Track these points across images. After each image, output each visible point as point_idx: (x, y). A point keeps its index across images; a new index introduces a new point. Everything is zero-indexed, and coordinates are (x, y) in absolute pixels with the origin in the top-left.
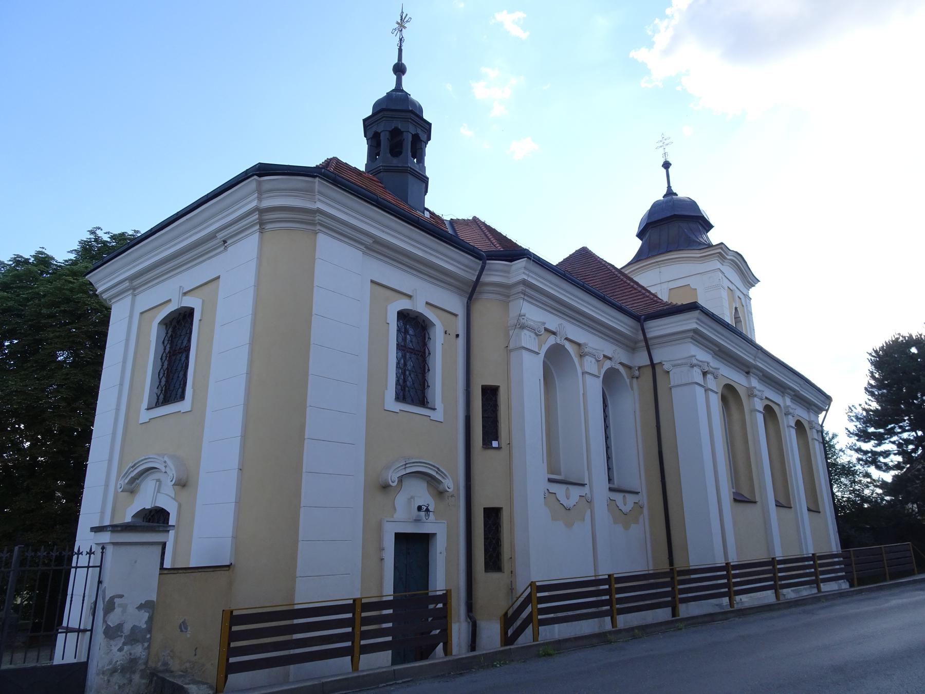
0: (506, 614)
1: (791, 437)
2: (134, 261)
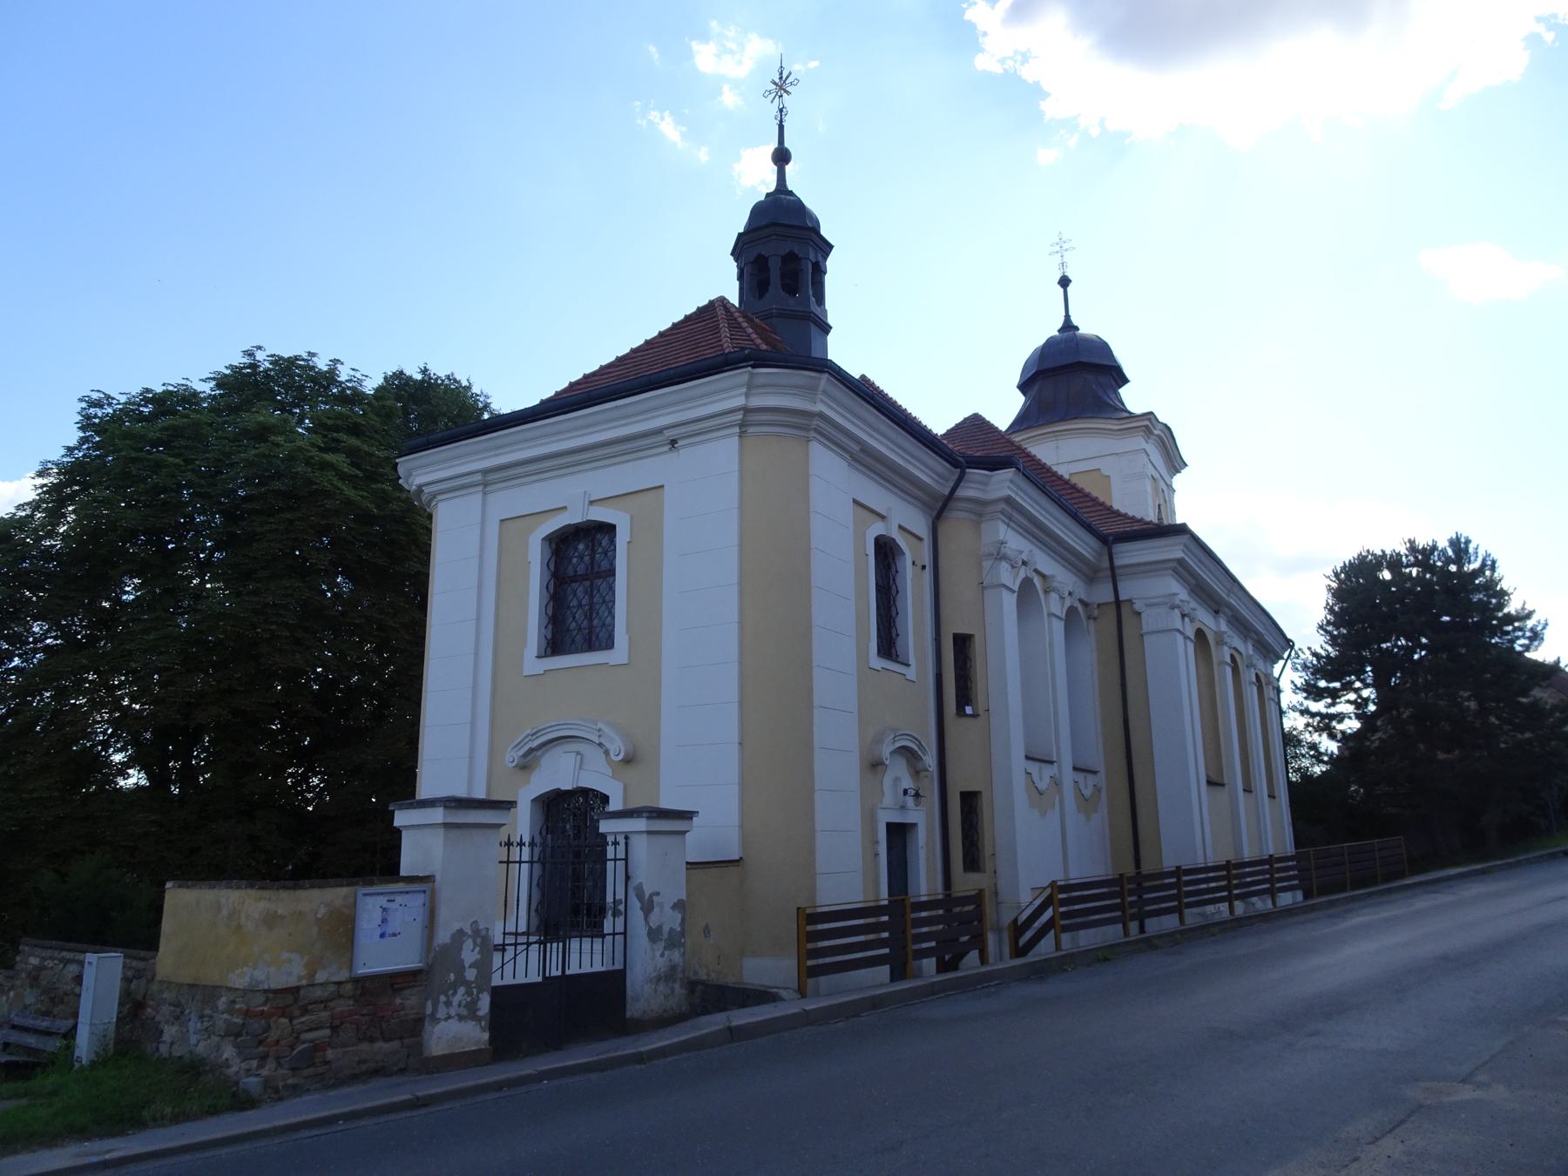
0: (1016, 920)
1: (1251, 693)
2: (497, 448)
